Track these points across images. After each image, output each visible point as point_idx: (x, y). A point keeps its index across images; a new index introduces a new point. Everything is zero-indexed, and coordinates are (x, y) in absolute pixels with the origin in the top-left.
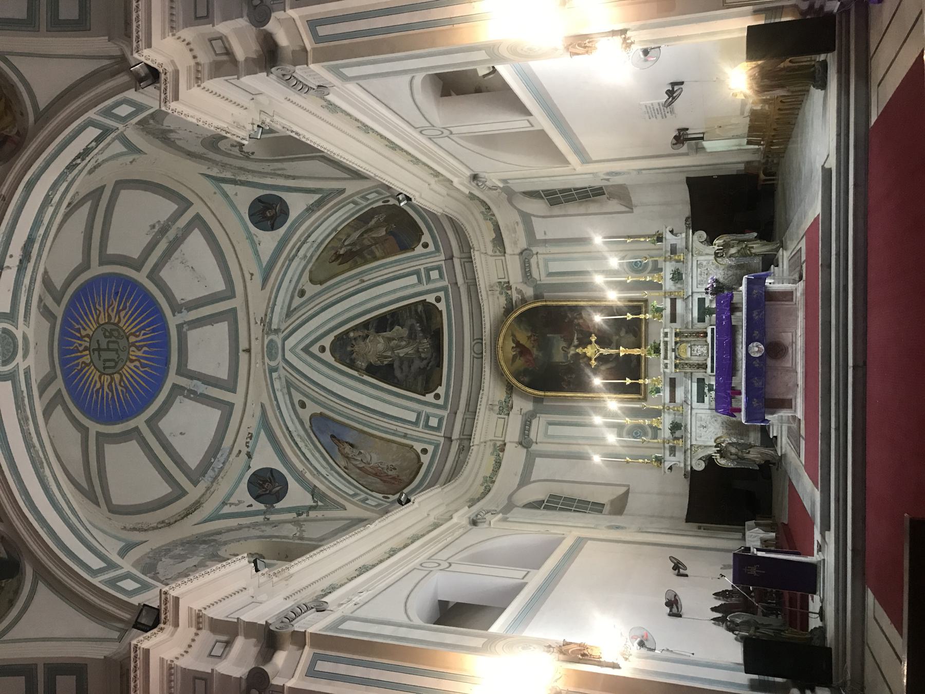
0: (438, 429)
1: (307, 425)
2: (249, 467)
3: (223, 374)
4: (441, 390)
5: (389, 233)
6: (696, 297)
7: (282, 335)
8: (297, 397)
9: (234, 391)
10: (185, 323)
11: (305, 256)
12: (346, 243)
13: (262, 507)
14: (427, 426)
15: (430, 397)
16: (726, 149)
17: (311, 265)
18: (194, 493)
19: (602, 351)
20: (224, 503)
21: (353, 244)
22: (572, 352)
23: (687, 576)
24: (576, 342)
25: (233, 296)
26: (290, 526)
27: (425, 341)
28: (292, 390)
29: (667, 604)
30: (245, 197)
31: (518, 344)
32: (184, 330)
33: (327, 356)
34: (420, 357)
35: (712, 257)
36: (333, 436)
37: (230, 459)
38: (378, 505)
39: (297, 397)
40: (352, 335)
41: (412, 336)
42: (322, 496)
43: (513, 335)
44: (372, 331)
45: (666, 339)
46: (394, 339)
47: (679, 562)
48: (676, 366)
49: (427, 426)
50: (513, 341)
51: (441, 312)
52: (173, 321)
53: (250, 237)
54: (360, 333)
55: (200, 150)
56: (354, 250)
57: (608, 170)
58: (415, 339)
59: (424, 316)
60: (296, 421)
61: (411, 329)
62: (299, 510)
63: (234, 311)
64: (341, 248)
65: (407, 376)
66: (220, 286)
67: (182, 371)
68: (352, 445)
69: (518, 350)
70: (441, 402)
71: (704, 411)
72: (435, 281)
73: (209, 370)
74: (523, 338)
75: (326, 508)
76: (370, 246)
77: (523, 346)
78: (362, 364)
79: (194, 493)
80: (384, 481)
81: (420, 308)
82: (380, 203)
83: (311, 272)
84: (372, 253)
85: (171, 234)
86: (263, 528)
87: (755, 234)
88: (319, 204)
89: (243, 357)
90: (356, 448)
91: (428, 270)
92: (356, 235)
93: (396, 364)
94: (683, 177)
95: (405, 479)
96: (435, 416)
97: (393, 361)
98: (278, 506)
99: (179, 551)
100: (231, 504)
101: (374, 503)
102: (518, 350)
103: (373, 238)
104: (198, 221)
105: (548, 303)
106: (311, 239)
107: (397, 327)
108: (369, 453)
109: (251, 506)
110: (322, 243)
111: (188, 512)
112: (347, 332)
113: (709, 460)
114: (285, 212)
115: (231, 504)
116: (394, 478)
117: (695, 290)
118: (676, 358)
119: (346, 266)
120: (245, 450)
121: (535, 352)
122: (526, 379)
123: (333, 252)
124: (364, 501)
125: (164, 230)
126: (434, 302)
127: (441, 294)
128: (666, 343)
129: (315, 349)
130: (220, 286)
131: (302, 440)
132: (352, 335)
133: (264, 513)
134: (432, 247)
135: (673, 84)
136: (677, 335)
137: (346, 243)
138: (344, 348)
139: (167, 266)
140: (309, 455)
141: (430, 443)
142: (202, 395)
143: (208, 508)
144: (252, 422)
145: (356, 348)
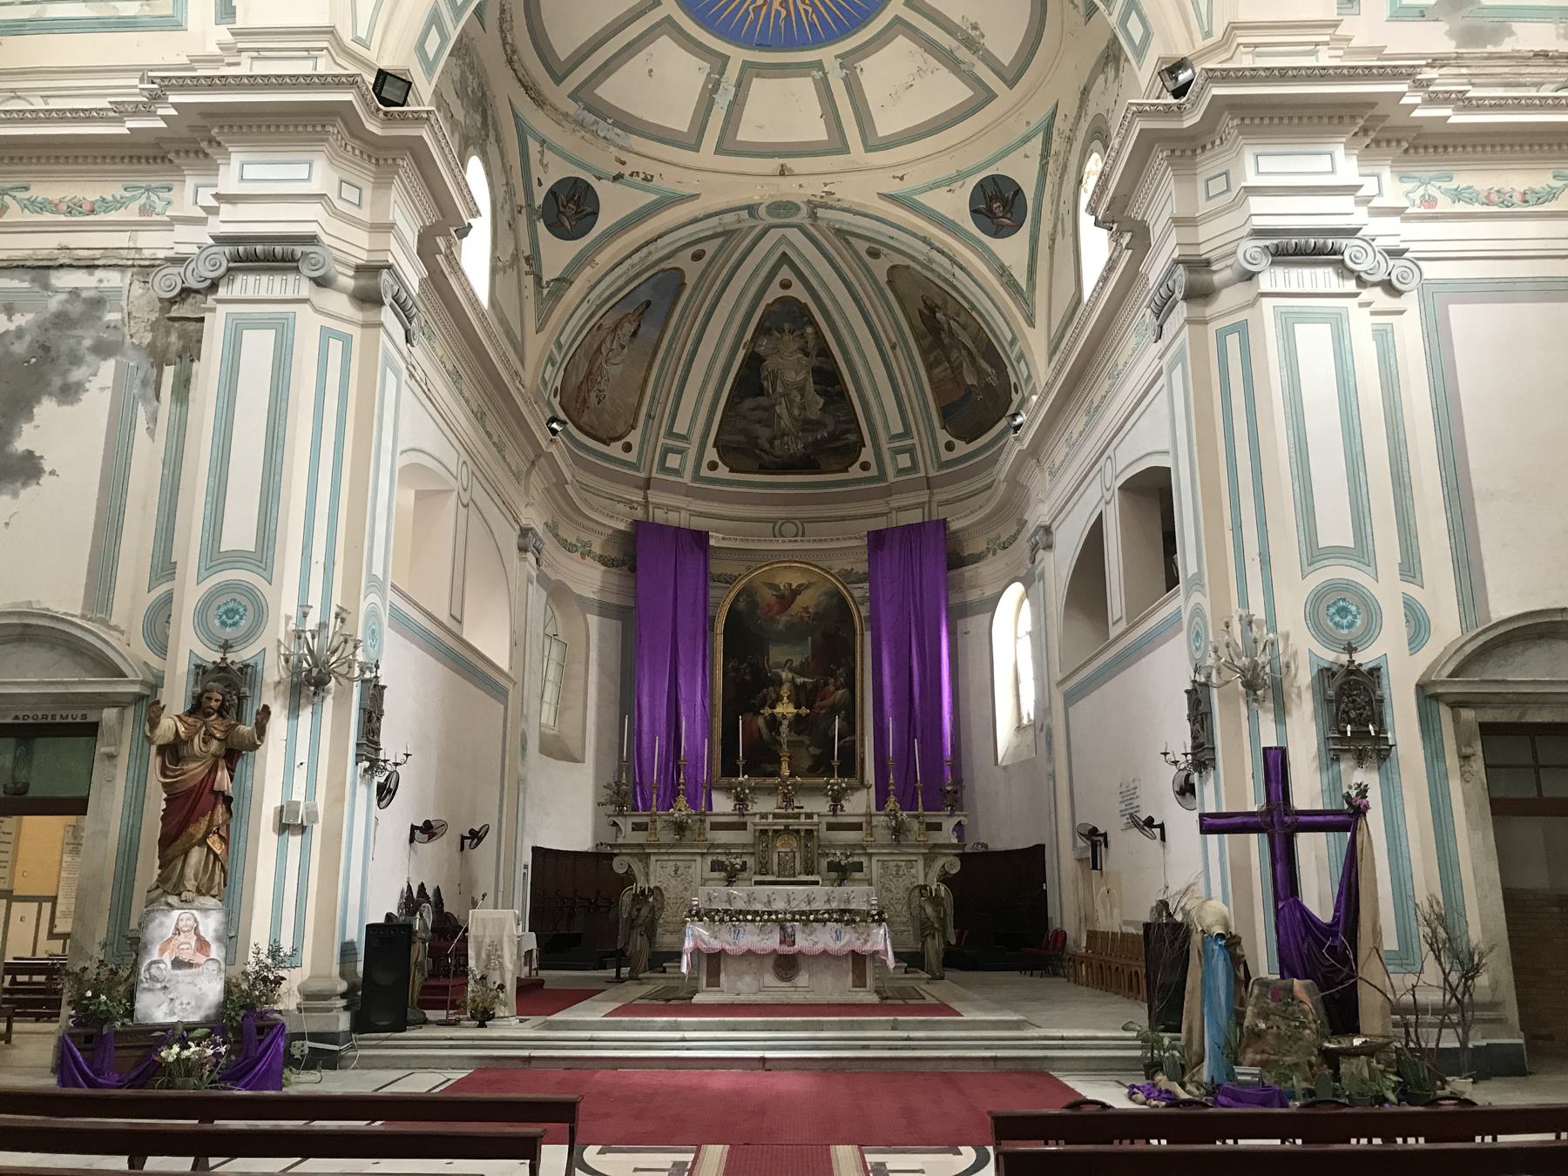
1: (666, 265)
2: (599, 179)
3: (745, 134)
4: (723, 472)
5: (969, 390)
6: (864, 860)
7: (807, 223)
8: (710, 248)
9: (719, 150)
10: (825, 74)
13: (539, 201)
15: (711, 454)
16: (1069, 903)
17: (918, 268)
18: (559, 95)
19: (786, 723)
20: (543, 142)
21: (951, 332)
22: (784, 675)
23: (462, 848)
24: (799, 680)
25: (869, 148)
26: (511, 250)
28: (719, 241)
29: (472, 832)
30: (1022, 170)
31: (795, 593)
32: (814, 73)
34: (774, 438)
36: (648, 303)
37: (612, 149)
38: (545, 383)
39: (710, 248)
40: (809, 330)
41: (808, 425)
42: (556, 296)
43: (809, 586)
44: (815, 362)
46: (802, 396)
47: (480, 839)
49: (667, 450)
52: (827, 55)
53: (961, 176)
54: (810, 345)
55: (1092, 110)
57: (1055, 732)
58: (803, 430)
60: (673, 247)
61: (818, 424)
62: (533, 260)
63: (845, 149)
66: (884, 128)
67: (750, 71)
68: (634, 334)
69: (787, 593)
72: (894, 460)
73: (750, 112)
74: (807, 600)
78: (764, 346)
79: (559, 95)
80: (579, 388)
81: (852, 437)
82: (1013, 380)
83: (908, 267)
84: (938, 363)
85: (963, 54)
86: (507, 207)
87: (953, 942)
88: (1010, 284)
89: (773, 164)
90: (631, 342)
93: (762, 400)
98: (541, 225)
99: (473, 83)
100: (542, 153)
101: (547, 376)
102: (787, 593)
104: (986, 97)
106: (957, 271)
107: (822, 401)
109: (540, 184)
111: (529, 88)
112: (812, 322)
113: (629, 878)
114: (999, 232)
115: (542, 153)
116: (585, 401)
117: (874, 859)
118: (776, 831)
119: (917, 320)
120: (626, 171)
121: (784, 619)
122: (742, 606)
123: (939, 303)
124: (551, 360)
125: (971, 43)
126: (861, 459)
127: (873, 471)
128: (797, 816)
129: (786, 273)
130: (884, 128)
131: (642, 260)
132: (809, 330)
133: (530, 205)
134: (946, 456)
135: (1162, 826)
136: (809, 832)
138: (788, 318)
139: (914, 47)
140: (618, 271)
141: (639, 459)
142: (712, 102)
143: (538, 120)
144: (669, 180)
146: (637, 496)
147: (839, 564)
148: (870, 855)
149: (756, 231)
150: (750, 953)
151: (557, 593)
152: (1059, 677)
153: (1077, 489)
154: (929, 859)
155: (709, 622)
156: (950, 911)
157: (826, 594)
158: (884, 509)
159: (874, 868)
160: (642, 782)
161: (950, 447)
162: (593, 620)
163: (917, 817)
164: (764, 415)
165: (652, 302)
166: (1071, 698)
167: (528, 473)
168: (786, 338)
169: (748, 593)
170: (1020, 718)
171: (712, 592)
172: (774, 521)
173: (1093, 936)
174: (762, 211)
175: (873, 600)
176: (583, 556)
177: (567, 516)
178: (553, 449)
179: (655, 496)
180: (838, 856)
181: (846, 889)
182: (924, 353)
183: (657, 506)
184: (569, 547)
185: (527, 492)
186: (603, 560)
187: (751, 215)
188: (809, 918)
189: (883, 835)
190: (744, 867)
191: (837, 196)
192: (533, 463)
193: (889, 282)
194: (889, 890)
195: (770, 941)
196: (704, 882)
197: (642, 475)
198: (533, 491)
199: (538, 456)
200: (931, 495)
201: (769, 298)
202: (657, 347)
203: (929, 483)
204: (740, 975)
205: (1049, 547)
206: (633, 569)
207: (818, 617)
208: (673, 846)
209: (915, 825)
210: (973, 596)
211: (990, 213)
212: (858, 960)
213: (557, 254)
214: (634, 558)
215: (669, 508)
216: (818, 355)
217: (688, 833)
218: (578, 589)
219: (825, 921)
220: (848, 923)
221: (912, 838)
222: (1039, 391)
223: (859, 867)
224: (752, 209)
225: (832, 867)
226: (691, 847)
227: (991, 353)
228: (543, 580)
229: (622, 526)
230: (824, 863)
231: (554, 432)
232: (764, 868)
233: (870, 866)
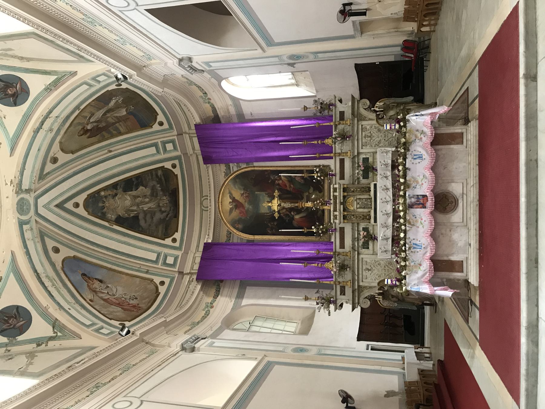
0: (173, 266)
4: (177, 235)
5: (129, 113)
6: (362, 156)
11: (51, 130)
12: (91, 120)
14: (165, 263)
15: (168, 241)
19: (283, 204)
27: (165, 198)
28: (47, 239)
29: (343, 402)
31: (234, 200)
33: (81, 211)
34: (161, 210)
35: (374, 122)
36: (84, 275)
40: (103, 193)
41: (154, 194)
43: (230, 193)
44: (120, 190)
45: (335, 194)
47: (350, 397)
48: (345, 217)
49: (165, 263)
50: (230, 198)
51: (176, 176)
56: (100, 126)
58: (157, 196)
59: (163, 178)
61: (153, 189)
62: (39, 342)
64: (88, 124)
65: (150, 225)
68: (101, 281)
70: (177, 244)
71: (369, 256)
74: (238, 194)
75: (65, 337)
76: (114, 124)
77: (237, 201)
80: (125, 310)
81: (160, 173)
83: (60, 143)
84: (117, 129)
88: (56, 84)
91: (164, 143)
92: (99, 114)
93: (141, 216)
94: (351, 64)
95: (143, 306)
96: (171, 255)
97: (138, 213)
98: (20, 338)
102: (234, 204)
103: (116, 117)
105: (256, 168)
108: (116, 287)
110: (68, 117)
113: (372, 298)
116: (134, 306)
117: (361, 151)
121: (247, 205)
122: (240, 226)
123: (80, 127)
126: (170, 168)
127: (176, 162)
129: (69, 205)
132: (103, 193)
134: (166, 126)
136: (345, 190)
137: (91, 120)
138: (96, 204)
141: (167, 277)
145: (107, 204)
146: (187, 278)
147: (222, 178)
148: (359, 153)
149: (38, 219)
150: (434, 235)
151: (228, 323)
152: (260, 51)
153: (134, 27)
154: (361, 118)
155: (251, 243)
156: (392, 100)
157: (234, 185)
158: (194, 156)
159: (366, 151)
160: (324, 283)
161: (161, 124)
162: (245, 302)
163: (336, 126)
164: (148, 216)
165: (82, 274)
166: (270, 43)
167: (153, 345)
168: (107, 205)
169: (234, 224)
170: (292, 85)
171: (235, 241)
172: (202, 210)
173: (408, 17)
174: (24, 218)
175: (238, 161)
176: (212, 307)
177: (189, 317)
178: (138, 333)
179: (187, 270)
180: (359, 172)
181: (379, 166)
182: (112, 136)
183: (192, 268)
184: (207, 314)
185: (162, 346)
186: (216, 297)
187: (27, 222)
188: (399, 186)
189: (347, 146)
190: (366, 229)
191: (13, 178)
192: (147, 343)
193: (73, 153)
194: (380, 142)
195: (423, 217)
196: (375, 253)
197: (177, 275)
198: (163, 343)
199: (143, 341)
200: (186, 133)
201: (85, 214)
202: (110, 269)
203: (180, 134)
204: (452, 243)
205: (190, 59)
206: (222, 281)
207: (245, 188)
208: (353, 272)
209: (340, 127)
210: (232, 111)
211: (15, 96)
212: (438, 140)
213: (39, 328)
214: (216, 281)
215: (194, 262)
216: (117, 189)
217: (346, 263)
218: (228, 311)
219: (405, 169)
220: (407, 149)
221: (348, 129)
222: (109, 68)
223: (366, 160)
224: (21, 224)
225: (366, 176)
226: (354, 261)
227: (104, 99)
228: (214, 336)
229: (199, 287)
230: (363, 181)
231: (128, 332)
232: (366, 217)
233: (365, 153)
